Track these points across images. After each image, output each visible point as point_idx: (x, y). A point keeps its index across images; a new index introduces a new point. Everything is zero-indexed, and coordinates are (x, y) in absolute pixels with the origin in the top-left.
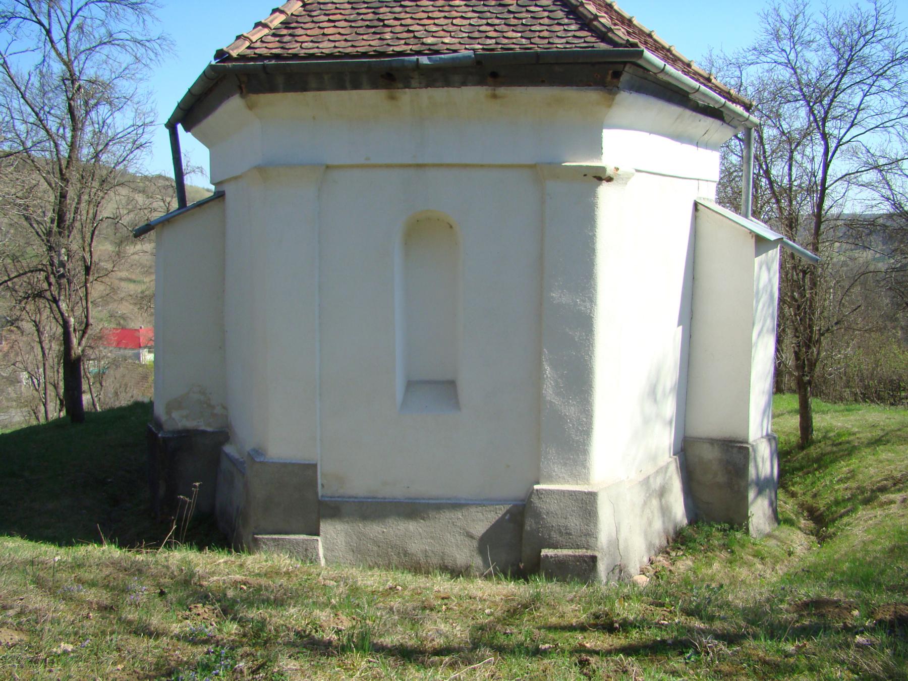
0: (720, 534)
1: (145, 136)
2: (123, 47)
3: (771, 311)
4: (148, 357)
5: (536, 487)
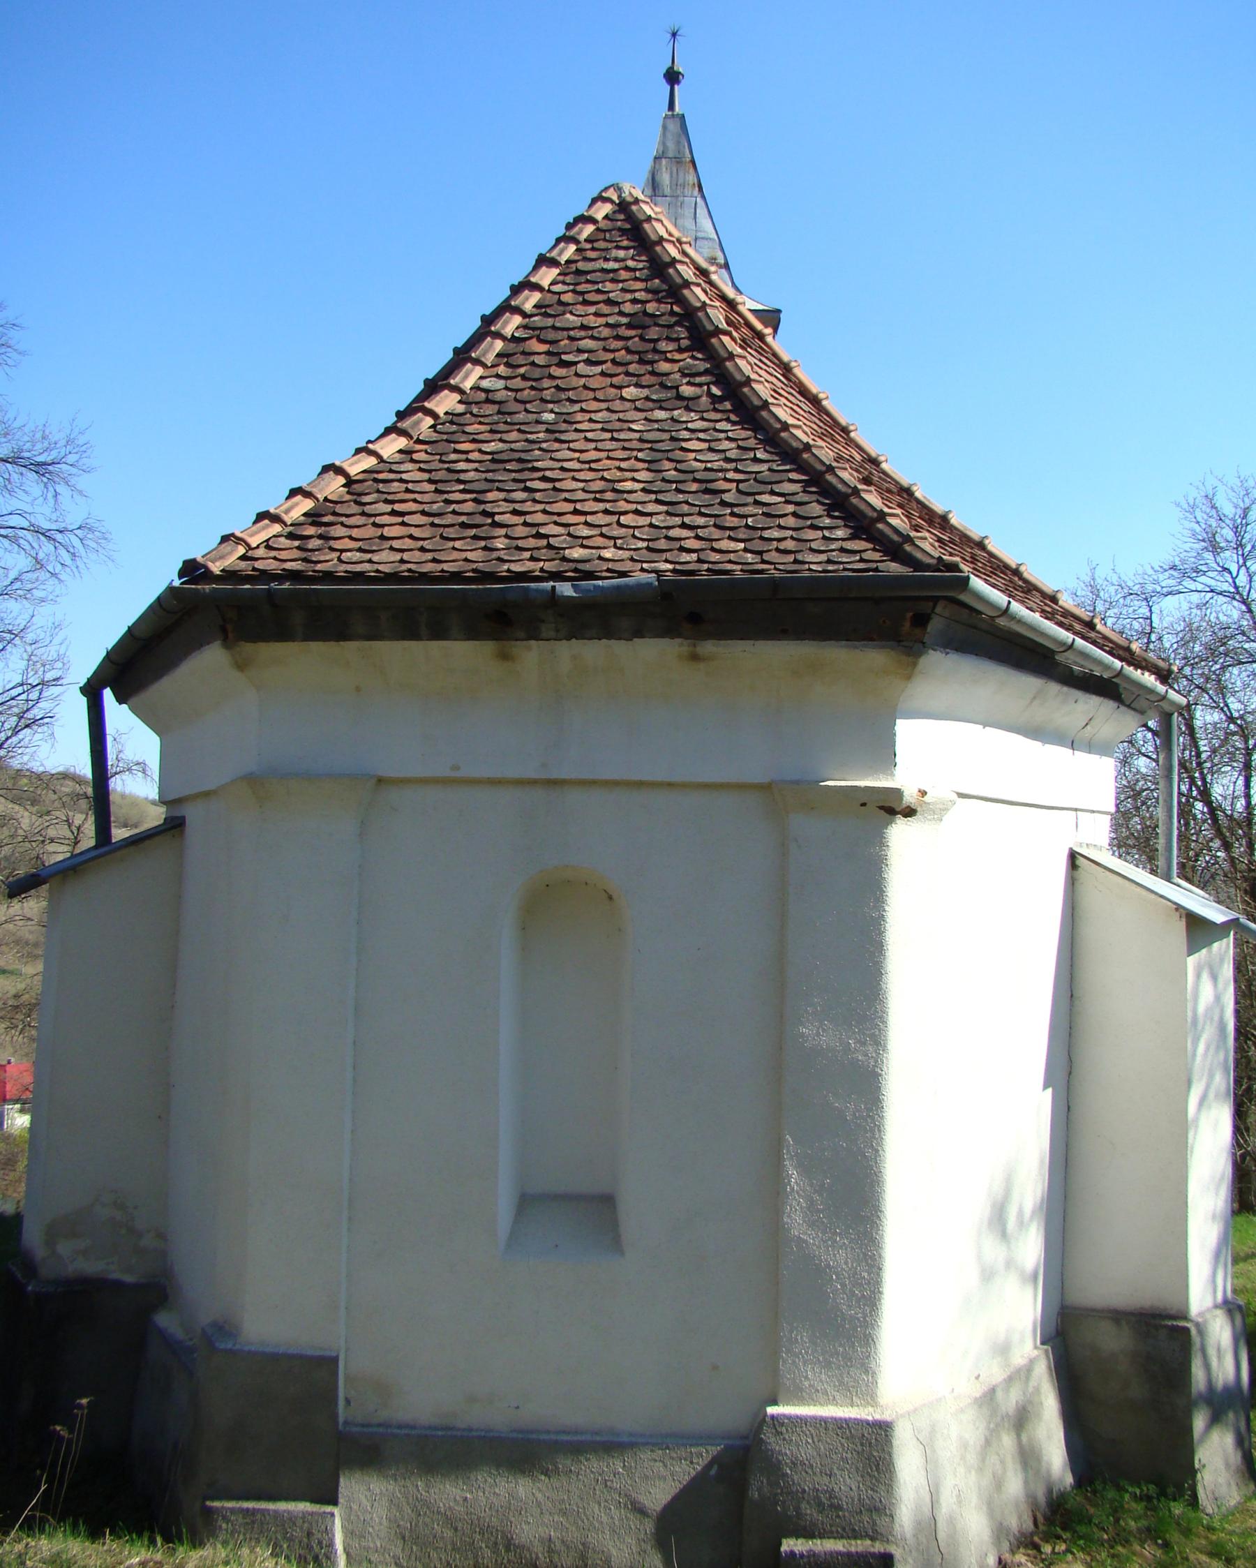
0: (1139, 1507)
1: (42, 705)
2: (14, 540)
3: (1221, 1056)
4: (19, 1121)
5: (771, 1410)
